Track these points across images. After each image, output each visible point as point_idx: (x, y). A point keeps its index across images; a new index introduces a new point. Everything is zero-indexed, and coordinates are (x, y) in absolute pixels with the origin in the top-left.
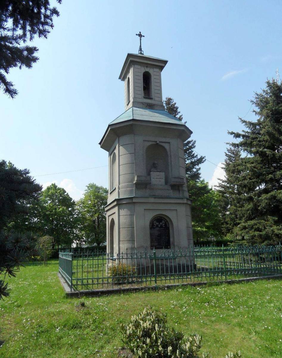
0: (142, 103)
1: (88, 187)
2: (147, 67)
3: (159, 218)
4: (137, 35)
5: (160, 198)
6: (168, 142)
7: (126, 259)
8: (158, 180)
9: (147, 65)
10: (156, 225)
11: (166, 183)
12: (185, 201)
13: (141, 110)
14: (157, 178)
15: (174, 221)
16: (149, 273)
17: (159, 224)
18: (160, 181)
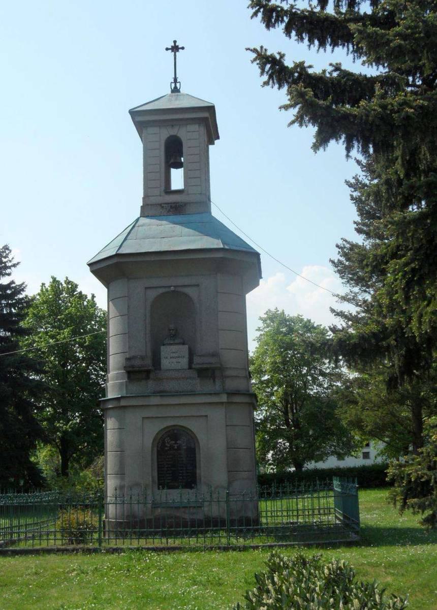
0: (160, 205)
1: (264, 321)
2: (172, 126)
3: (175, 432)
4: (167, 49)
5: (173, 396)
6: (197, 284)
7: (115, 505)
8: (174, 360)
9: (172, 123)
10: (169, 446)
11: (190, 368)
12: (224, 398)
13: (154, 221)
14: (173, 357)
15: (201, 437)
16: (213, 523)
17: (176, 443)
18: (179, 362)
